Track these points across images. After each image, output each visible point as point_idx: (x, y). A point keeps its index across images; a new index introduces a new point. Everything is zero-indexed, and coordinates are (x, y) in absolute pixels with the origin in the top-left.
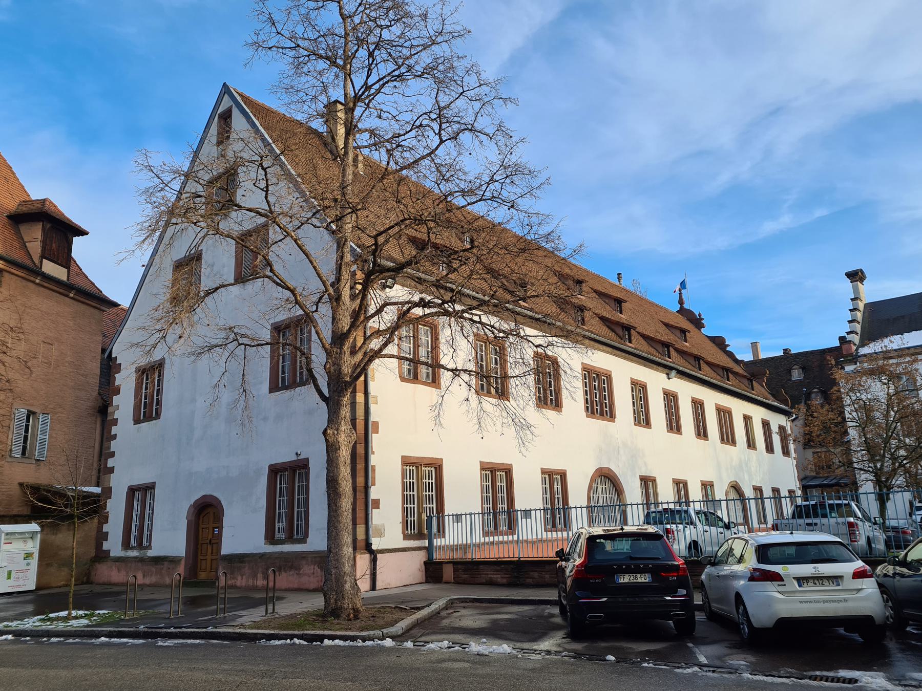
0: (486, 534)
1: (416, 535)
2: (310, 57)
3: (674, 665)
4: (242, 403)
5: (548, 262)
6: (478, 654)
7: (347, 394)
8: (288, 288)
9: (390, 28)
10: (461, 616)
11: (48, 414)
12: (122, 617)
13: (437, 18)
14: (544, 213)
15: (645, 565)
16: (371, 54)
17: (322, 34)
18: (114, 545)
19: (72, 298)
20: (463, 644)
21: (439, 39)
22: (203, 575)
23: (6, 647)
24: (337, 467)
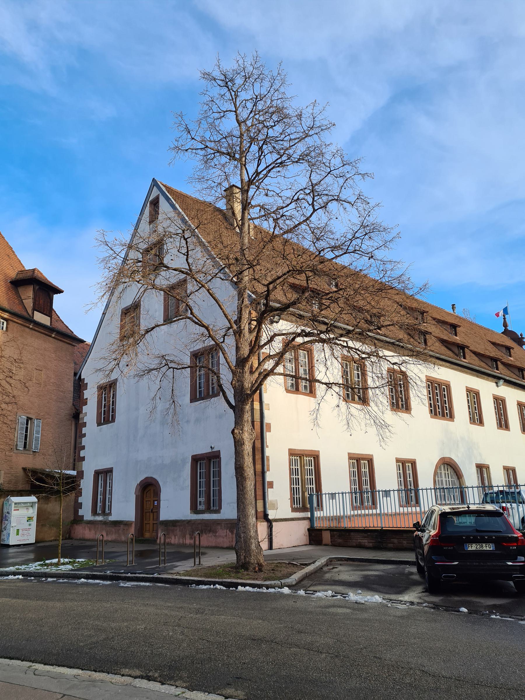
0: (354, 508)
1: (301, 508)
2: (215, 154)
3: (517, 617)
4: (172, 411)
5: (397, 298)
6: (356, 603)
7: (248, 403)
8: (203, 326)
9: (274, 128)
10: (339, 571)
11: (40, 419)
12: (95, 564)
13: (309, 117)
14: (396, 260)
15: (489, 537)
16: (261, 148)
17: (225, 136)
18: (86, 512)
19: (54, 338)
20: (343, 594)
21: (311, 132)
22: (147, 535)
23: (18, 584)
24: (243, 457)
